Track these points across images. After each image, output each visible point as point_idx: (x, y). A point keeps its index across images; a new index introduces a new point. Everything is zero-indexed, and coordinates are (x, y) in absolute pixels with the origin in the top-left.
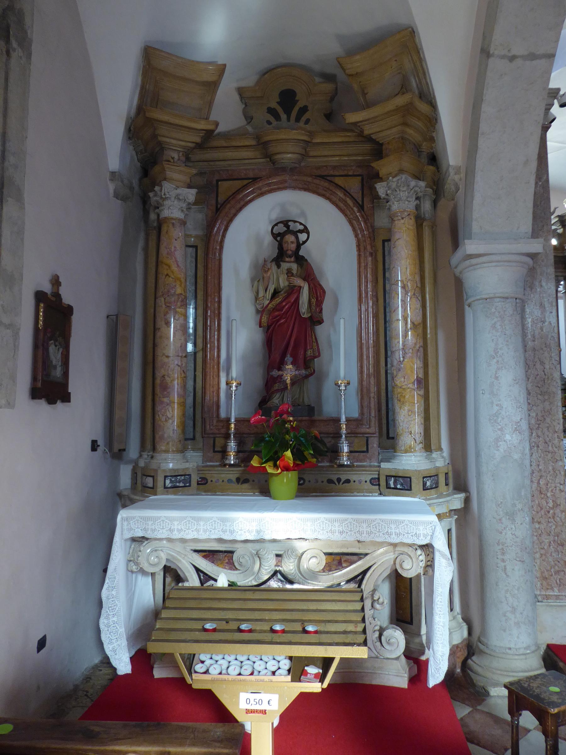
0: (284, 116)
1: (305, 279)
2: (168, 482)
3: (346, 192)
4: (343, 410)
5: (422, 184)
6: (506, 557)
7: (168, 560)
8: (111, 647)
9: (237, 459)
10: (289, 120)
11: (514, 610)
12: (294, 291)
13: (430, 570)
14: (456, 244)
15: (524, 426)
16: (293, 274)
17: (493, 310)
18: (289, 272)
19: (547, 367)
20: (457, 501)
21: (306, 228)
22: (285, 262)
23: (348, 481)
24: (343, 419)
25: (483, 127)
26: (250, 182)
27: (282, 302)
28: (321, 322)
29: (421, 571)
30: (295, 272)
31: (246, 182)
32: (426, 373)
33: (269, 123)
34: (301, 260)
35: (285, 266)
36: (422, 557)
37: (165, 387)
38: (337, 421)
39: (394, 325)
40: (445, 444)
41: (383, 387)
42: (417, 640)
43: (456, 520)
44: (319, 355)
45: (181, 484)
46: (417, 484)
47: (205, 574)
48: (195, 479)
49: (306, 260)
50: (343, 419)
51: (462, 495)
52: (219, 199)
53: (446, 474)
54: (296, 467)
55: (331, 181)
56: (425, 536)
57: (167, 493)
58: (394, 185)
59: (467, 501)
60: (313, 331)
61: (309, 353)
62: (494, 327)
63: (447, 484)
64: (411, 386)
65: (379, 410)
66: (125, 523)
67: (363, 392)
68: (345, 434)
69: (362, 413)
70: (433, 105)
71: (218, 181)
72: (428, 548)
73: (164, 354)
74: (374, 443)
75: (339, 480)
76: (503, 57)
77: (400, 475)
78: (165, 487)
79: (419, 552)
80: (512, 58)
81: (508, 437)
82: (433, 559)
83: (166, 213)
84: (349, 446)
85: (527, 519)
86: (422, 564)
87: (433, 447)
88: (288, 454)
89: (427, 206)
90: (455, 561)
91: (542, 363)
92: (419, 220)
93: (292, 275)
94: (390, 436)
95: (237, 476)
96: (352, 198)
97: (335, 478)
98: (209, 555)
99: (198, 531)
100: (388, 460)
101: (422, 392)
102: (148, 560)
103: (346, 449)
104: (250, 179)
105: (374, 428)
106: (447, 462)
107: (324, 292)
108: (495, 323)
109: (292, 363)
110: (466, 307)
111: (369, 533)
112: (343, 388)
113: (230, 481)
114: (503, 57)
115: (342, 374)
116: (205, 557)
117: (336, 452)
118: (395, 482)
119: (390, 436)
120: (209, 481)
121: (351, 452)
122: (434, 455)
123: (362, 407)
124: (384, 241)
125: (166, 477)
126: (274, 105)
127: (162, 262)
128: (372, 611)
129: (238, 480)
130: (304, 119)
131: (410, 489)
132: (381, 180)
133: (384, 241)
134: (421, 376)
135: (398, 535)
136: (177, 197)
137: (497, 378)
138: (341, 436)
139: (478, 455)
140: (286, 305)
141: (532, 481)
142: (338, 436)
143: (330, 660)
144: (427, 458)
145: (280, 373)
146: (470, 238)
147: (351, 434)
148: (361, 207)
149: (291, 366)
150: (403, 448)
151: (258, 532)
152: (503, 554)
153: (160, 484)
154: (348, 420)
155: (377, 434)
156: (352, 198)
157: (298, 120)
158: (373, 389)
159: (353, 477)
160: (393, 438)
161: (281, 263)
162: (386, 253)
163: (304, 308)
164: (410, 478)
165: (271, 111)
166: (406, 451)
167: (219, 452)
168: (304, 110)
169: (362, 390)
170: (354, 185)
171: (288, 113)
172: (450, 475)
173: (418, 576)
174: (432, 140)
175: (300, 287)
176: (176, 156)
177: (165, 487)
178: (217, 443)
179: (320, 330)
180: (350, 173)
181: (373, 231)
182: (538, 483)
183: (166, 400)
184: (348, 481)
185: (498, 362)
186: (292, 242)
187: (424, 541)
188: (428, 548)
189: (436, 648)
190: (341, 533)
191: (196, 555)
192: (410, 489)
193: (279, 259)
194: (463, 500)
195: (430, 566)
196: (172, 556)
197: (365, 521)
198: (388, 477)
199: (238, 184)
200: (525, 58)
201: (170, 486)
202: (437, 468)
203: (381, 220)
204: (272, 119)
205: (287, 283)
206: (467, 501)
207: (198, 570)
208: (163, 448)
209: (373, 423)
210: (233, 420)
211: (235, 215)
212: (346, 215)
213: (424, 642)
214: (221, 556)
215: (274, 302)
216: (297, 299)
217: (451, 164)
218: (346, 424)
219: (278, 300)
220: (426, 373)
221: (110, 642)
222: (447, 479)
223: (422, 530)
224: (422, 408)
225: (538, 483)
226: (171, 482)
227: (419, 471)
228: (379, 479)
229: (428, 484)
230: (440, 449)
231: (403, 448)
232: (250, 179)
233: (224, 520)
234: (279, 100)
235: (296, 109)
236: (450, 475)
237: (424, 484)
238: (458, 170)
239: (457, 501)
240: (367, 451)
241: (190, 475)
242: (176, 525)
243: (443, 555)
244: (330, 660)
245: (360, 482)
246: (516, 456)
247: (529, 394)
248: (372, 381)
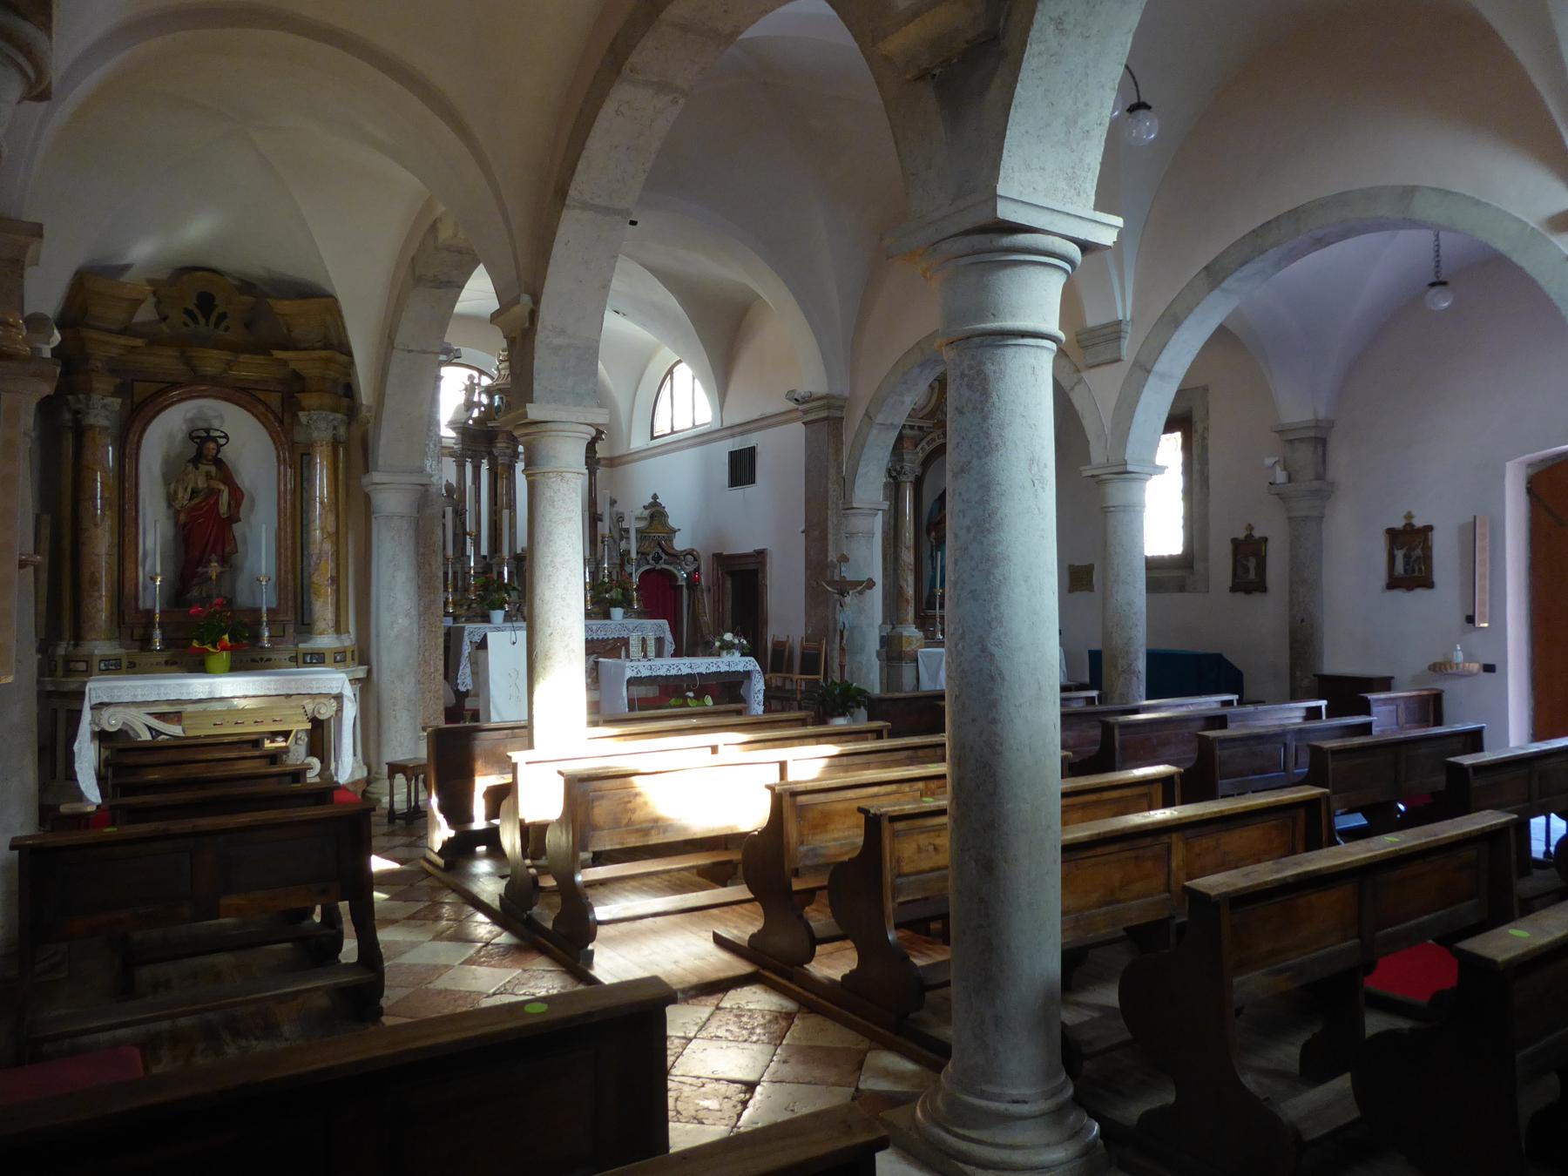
0: (202, 321)
1: (225, 483)
2: (102, 665)
3: (267, 407)
4: (264, 602)
5: (339, 416)
6: (396, 708)
7: (124, 723)
8: (84, 785)
9: (163, 645)
10: (207, 323)
11: (401, 745)
12: (213, 494)
13: (339, 713)
14: (367, 470)
15: (413, 612)
16: (211, 476)
17: (392, 525)
18: (208, 475)
19: (434, 567)
20: (361, 672)
21: (226, 435)
22: (202, 464)
23: (269, 660)
24: (264, 609)
25: (388, 391)
26: (166, 388)
27: (201, 502)
28: (238, 520)
29: (333, 713)
30: (214, 474)
31: (164, 385)
32: (338, 572)
33: (186, 324)
34: (218, 463)
35: (204, 468)
36: (335, 704)
37: (95, 583)
38: (258, 611)
39: (313, 533)
40: (352, 628)
41: (299, 582)
42: (328, 773)
43: (360, 688)
44: (237, 552)
45: (113, 668)
46: (329, 658)
47: (155, 730)
48: (125, 663)
49: (224, 463)
50: (264, 609)
51: (365, 667)
52: (135, 399)
53: (353, 651)
54: (231, 649)
55: (254, 395)
56: (337, 688)
57: (102, 674)
58: (315, 417)
59: (369, 672)
60: (231, 529)
61: (227, 549)
62: (393, 537)
63: (353, 659)
64: (326, 583)
65: (295, 601)
66: (92, 692)
67: (281, 586)
68: (267, 622)
69: (279, 604)
70: (350, 354)
71: (133, 381)
72: (339, 698)
73: (93, 553)
74: (290, 629)
75: (261, 659)
76: (403, 350)
77: (316, 652)
78: (100, 670)
79: (332, 700)
80: (410, 351)
81: (400, 621)
82: (342, 705)
83: (91, 420)
84: (270, 631)
85: (413, 680)
86: (335, 709)
87: (342, 631)
88: (226, 637)
89: (342, 431)
90: (358, 703)
91: (430, 565)
92: (335, 444)
93: (212, 478)
94: (305, 622)
95: (164, 659)
96: (273, 412)
97: (258, 657)
98: (161, 716)
99: (159, 694)
100: (305, 642)
101: (334, 587)
102: (109, 724)
103: (267, 634)
104: (167, 383)
105: (290, 616)
106: (353, 643)
107: (243, 495)
108: (393, 536)
109: (217, 562)
110: (373, 520)
111: (297, 689)
112: (264, 583)
113: (158, 664)
114: (403, 350)
115: (264, 571)
116: (156, 718)
117: (257, 637)
118: (311, 659)
119: (305, 622)
120: (137, 664)
121: (270, 637)
122: (344, 637)
123: (279, 599)
124: (302, 455)
125: (100, 661)
126: (191, 306)
127: (89, 468)
128: (296, 746)
129: (167, 663)
130: (223, 325)
131: (324, 662)
132: (303, 409)
133: (302, 455)
134: (334, 574)
135: (318, 688)
136: (104, 407)
137: (394, 577)
138: (262, 624)
139: (378, 636)
140: (205, 506)
141: (419, 654)
142: (259, 622)
143: (291, 732)
144: (338, 638)
145: (205, 570)
146: (376, 470)
147: (270, 623)
148: (281, 422)
149: (216, 564)
150: (318, 632)
151: (210, 692)
152: (395, 706)
153: (95, 669)
154: (269, 610)
155: (293, 622)
156: (273, 412)
157: (217, 325)
158: (290, 583)
159: (274, 656)
160: (309, 624)
161: (200, 465)
162: (304, 465)
163: (223, 508)
164: (324, 654)
165: (188, 312)
166: (321, 634)
167: (136, 640)
168: (223, 316)
169: (280, 585)
170: (275, 400)
171: (207, 317)
172: (356, 653)
173: (329, 719)
174: (349, 375)
175: (219, 490)
176: (99, 365)
177: (100, 670)
178: (135, 632)
179: (237, 528)
180: (272, 389)
181: (293, 445)
182: (424, 655)
183: (96, 594)
184: (269, 660)
185: (395, 565)
186: (213, 449)
187: (335, 691)
188: (339, 698)
189: (343, 759)
190: (275, 689)
191: (149, 718)
192: (324, 662)
193: (197, 460)
194: (366, 671)
195: (340, 710)
196: (128, 720)
197: (293, 680)
198: (305, 655)
199: (154, 387)
200: (419, 352)
201: (104, 668)
202: (345, 647)
203: (300, 436)
204: (189, 321)
205: (205, 485)
206: (369, 672)
207: (150, 729)
208: (93, 637)
209: (289, 613)
210: (157, 611)
211: (154, 417)
212: (267, 428)
213: (333, 772)
214: (171, 716)
215: (193, 503)
216: (217, 501)
217: (364, 402)
218: (637, 586)
219: (196, 501)
220: (338, 572)
221: (84, 782)
222: (353, 655)
223: (335, 684)
224: (334, 601)
225: (424, 655)
226: (105, 665)
227: (332, 649)
228: (296, 657)
229: (338, 658)
230: (348, 632)
231: (318, 632)
232: (167, 383)
233: (181, 686)
234: (196, 302)
235: (215, 314)
236: (356, 653)
237: (335, 658)
238: (369, 408)
239: (361, 672)
240: (284, 636)
241: (120, 659)
242: (139, 692)
243: (350, 700)
244: (291, 732)
245: (280, 660)
246: (406, 635)
247: (419, 588)
248: (290, 576)
